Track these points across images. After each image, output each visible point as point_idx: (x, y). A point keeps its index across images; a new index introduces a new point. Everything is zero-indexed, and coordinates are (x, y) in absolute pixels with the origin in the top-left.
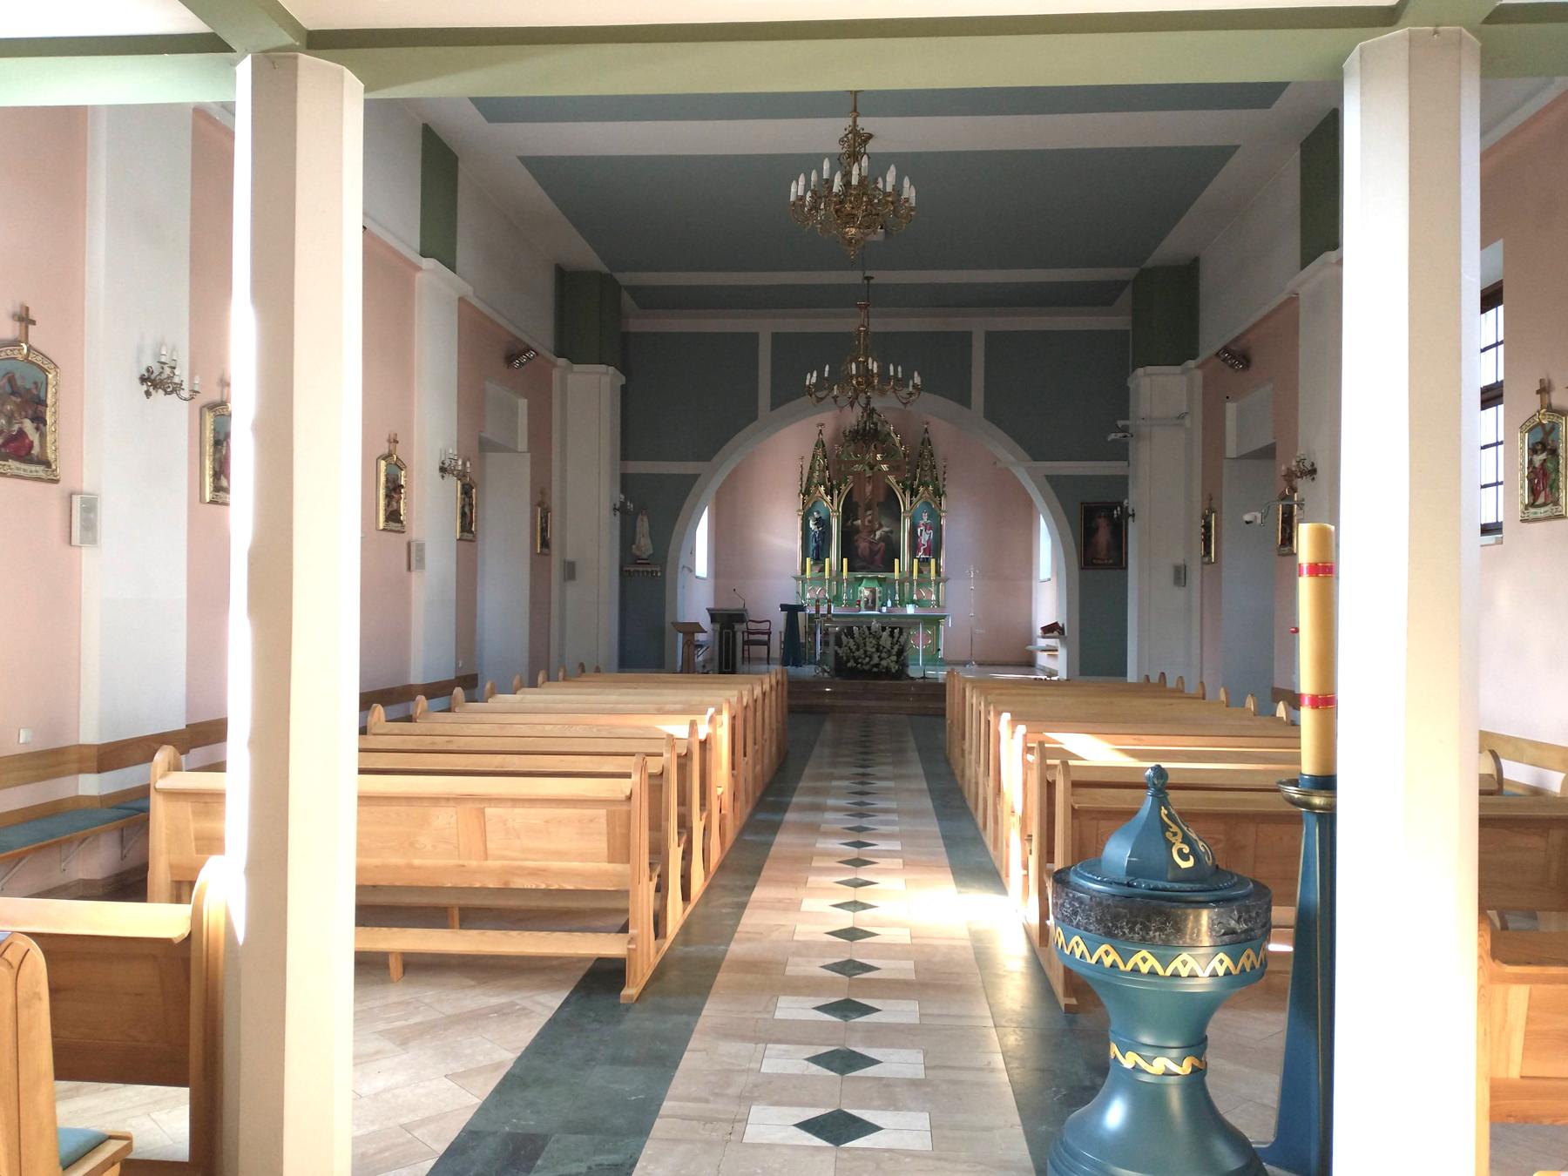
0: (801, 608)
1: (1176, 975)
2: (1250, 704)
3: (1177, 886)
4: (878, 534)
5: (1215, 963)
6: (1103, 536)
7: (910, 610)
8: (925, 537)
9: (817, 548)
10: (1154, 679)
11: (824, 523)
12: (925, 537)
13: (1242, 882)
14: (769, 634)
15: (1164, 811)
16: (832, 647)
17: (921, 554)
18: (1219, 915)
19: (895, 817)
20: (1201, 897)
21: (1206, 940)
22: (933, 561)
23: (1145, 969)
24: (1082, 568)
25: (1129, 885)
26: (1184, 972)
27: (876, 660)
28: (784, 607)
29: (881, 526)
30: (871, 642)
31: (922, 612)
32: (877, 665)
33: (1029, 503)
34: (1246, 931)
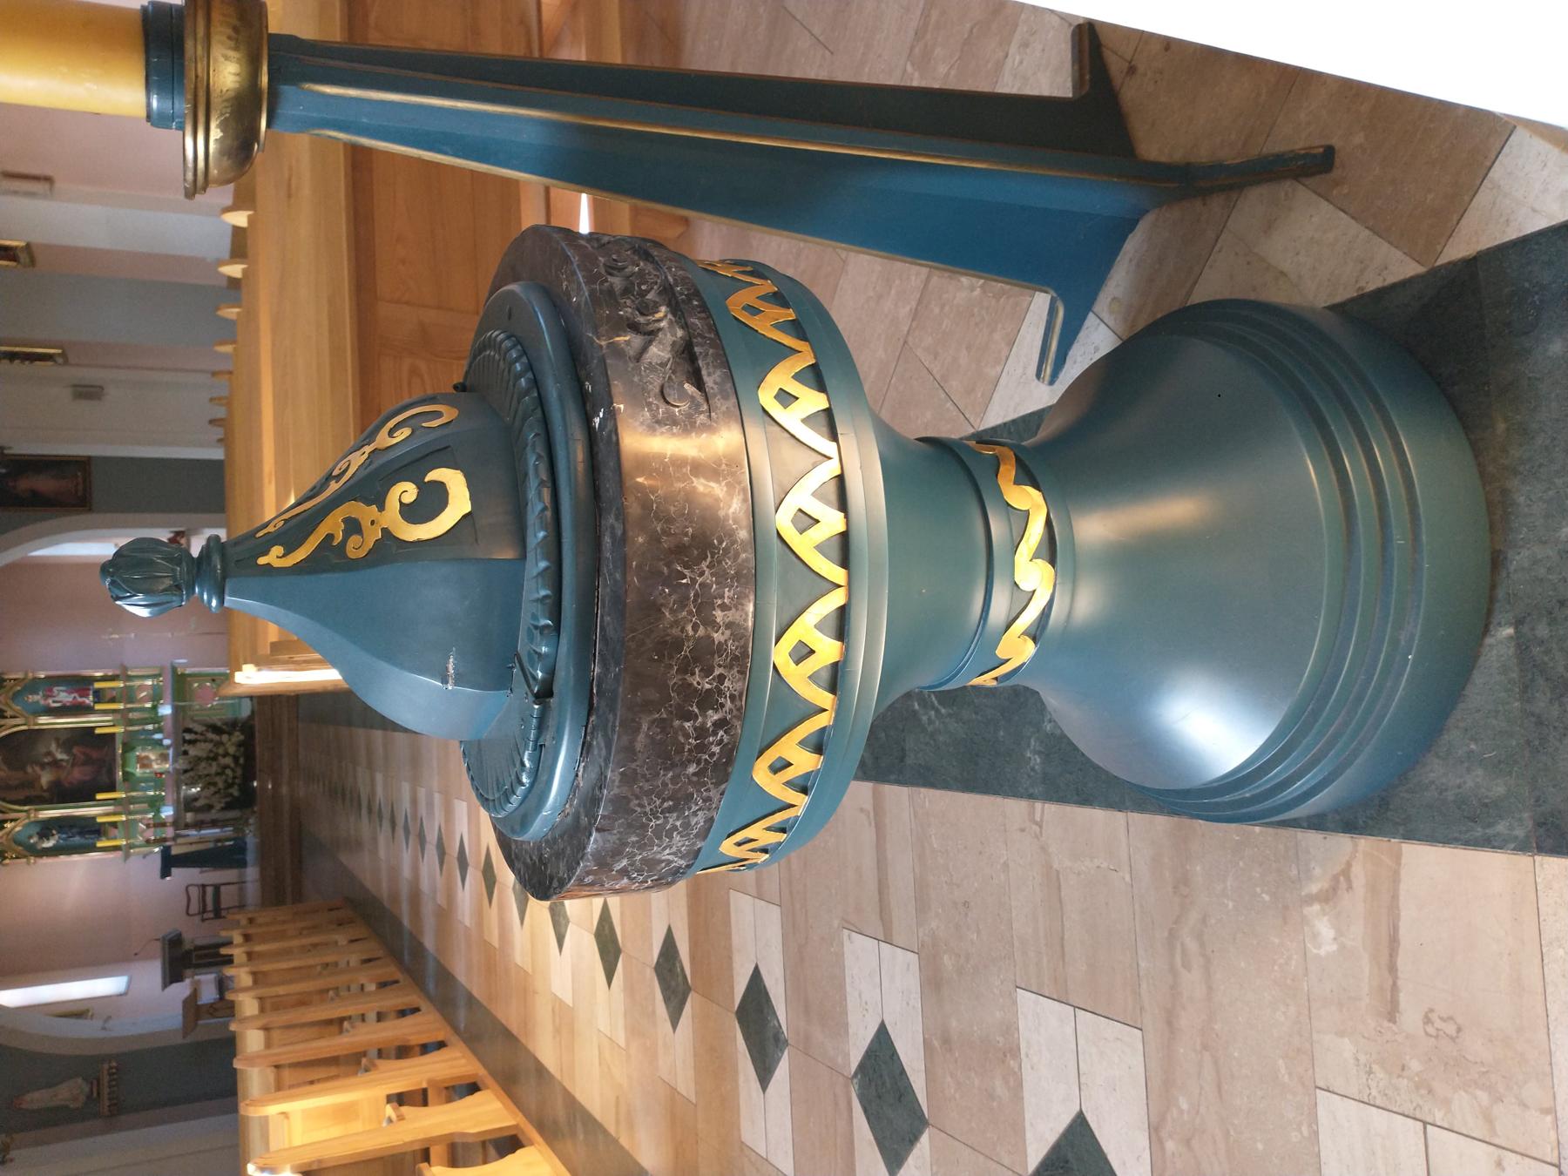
0: (166, 854)
1: (843, 550)
2: (231, 313)
3: (538, 536)
4: (60, 756)
5: (791, 418)
6: (45, 484)
7: (166, 710)
8: (64, 696)
9: (81, 834)
10: (218, 432)
11: (46, 828)
12: (64, 696)
13: (500, 313)
14: (204, 886)
15: (273, 557)
16: (213, 814)
17: (89, 700)
18: (638, 397)
19: (422, 793)
20: (573, 454)
21: (724, 440)
22: (97, 685)
23: (828, 651)
24: (90, 510)
25: (545, 694)
26: (832, 522)
27: (228, 761)
28: (165, 872)
29: (49, 754)
30: (203, 768)
31: (168, 694)
32: (236, 759)
33: (12, 568)
34: (675, 308)
